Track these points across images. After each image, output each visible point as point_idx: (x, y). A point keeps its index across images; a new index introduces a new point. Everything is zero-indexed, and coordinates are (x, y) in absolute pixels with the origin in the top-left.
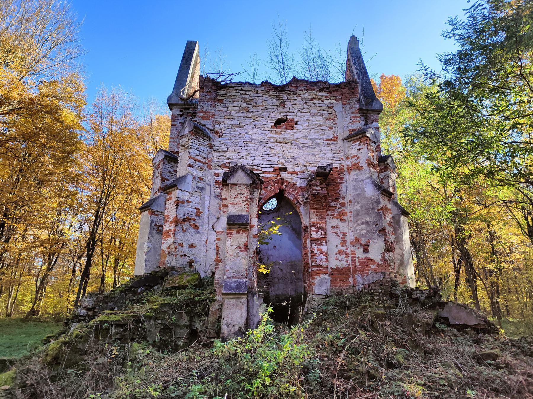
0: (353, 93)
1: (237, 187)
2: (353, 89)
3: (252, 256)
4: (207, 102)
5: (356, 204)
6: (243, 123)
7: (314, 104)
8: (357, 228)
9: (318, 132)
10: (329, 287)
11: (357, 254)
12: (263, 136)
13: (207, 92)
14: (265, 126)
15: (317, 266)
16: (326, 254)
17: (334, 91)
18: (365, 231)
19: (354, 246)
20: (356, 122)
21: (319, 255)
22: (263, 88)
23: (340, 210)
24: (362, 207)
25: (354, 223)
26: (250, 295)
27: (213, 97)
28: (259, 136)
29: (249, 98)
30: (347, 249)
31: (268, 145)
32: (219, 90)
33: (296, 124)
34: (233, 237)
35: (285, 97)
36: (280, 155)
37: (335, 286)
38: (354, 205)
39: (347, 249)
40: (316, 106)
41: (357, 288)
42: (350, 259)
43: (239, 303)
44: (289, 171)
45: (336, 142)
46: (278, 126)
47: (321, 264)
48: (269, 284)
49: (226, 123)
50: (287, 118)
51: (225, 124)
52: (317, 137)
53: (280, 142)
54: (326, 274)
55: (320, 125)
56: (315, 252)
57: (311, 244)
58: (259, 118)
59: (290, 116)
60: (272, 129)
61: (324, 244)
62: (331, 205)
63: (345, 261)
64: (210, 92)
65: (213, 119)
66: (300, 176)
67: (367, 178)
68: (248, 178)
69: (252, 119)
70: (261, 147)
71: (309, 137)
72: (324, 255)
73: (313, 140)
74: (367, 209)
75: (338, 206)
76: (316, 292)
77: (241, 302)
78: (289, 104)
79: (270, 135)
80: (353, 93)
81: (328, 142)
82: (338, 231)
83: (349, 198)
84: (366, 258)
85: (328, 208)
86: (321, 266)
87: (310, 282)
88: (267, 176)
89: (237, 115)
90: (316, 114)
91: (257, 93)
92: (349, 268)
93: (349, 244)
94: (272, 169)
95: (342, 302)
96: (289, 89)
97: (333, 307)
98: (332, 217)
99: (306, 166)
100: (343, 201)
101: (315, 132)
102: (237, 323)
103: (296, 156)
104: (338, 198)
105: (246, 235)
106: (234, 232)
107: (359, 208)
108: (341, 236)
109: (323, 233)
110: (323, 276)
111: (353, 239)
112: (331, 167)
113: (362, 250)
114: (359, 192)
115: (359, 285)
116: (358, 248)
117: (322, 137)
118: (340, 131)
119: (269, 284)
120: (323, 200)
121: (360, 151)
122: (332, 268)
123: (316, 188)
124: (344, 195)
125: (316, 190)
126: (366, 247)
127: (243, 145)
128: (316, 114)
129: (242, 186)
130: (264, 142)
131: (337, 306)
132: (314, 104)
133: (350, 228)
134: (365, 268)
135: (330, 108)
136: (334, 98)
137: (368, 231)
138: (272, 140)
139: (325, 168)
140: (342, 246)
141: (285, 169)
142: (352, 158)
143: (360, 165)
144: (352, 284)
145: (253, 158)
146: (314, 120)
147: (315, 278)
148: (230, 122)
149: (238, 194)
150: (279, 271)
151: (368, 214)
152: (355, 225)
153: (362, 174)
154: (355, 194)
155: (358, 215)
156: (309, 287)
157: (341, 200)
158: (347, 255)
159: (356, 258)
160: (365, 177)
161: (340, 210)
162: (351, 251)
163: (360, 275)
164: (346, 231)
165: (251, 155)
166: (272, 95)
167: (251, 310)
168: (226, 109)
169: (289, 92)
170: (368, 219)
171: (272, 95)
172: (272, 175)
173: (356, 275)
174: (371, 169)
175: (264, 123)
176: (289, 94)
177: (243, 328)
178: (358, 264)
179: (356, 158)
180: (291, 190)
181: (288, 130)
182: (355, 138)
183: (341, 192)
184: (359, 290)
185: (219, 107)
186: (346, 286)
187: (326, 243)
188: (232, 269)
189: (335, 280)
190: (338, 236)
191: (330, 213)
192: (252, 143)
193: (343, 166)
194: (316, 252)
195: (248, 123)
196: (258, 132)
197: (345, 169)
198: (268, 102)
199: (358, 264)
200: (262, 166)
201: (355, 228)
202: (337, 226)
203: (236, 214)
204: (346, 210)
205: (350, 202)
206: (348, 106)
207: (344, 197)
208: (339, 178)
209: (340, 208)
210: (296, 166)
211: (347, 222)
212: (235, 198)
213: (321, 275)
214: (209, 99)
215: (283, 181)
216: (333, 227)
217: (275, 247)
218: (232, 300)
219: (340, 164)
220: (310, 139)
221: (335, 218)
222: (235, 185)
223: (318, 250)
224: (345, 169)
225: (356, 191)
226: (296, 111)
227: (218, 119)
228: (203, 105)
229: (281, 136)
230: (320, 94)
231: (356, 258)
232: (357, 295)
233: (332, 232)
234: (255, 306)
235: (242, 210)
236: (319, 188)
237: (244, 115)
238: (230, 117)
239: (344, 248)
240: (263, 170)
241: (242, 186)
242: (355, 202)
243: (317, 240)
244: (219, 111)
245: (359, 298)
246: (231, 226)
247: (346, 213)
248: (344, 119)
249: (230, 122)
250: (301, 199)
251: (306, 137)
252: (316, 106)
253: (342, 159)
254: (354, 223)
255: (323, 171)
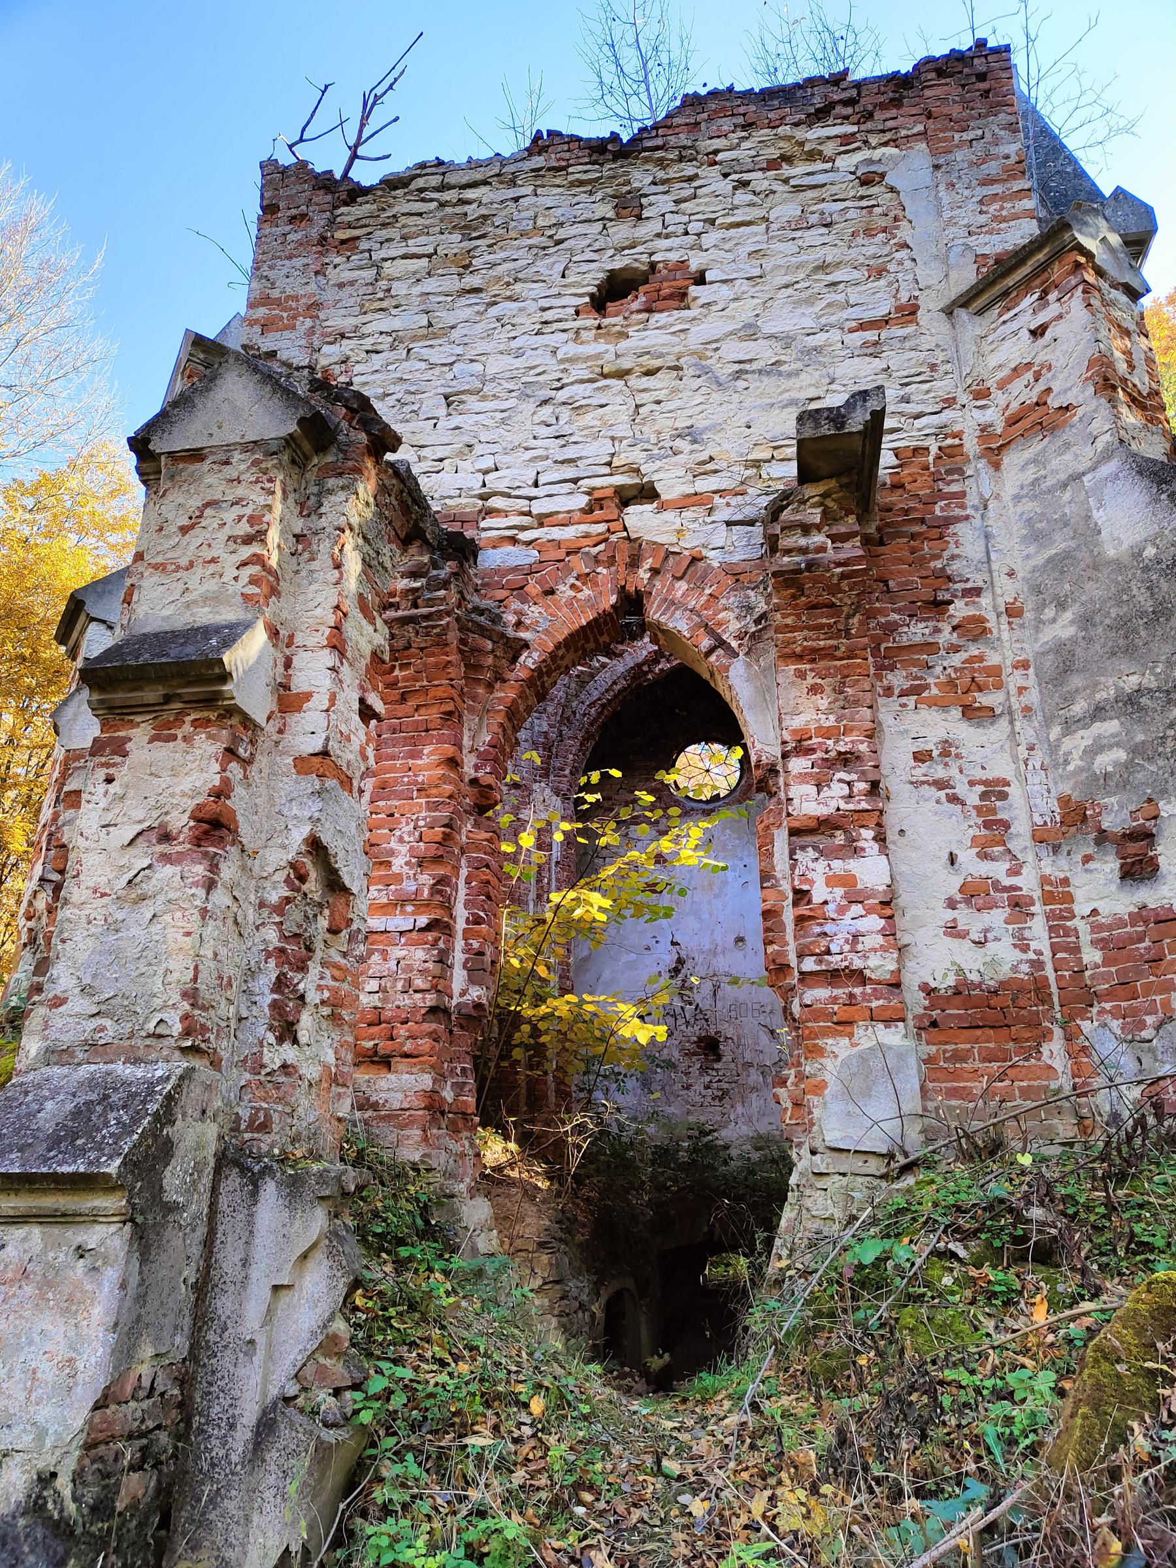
0: (986, 94)
1: (206, 466)
2: (982, 77)
3: (274, 897)
4: (290, 258)
5: (1049, 613)
6: (445, 317)
7: (786, 181)
8: (1067, 744)
9: (810, 301)
10: (912, 1103)
11: (1078, 894)
12: (542, 359)
13: (292, 220)
14: (548, 316)
15: (833, 976)
16: (887, 905)
17: (883, 106)
18: (1121, 755)
19: (1056, 849)
20: (1016, 217)
21: (842, 910)
22: (538, 161)
23: (957, 659)
24: (1086, 621)
25: (1048, 723)
26: (233, 1181)
27: (314, 232)
28: (518, 363)
29: (472, 211)
30: (1014, 872)
31: (562, 396)
32: (346, 204)
33: (700, 279)
34: (123, 774)
35: (640, 177)
36: (622, 430)
37: (953, 1093)
38: (1039, 624)
39: (1014, 872)
40: (799, 189)
41: (1103, 1102)
42: (1038, 930)
43: (63, 1256)
44: (664, 497)
45: (910, 329)
46: (611, 307)
47: (858, 963)
48: (725, 1093)
49: (366, 330)
50: (653, 266)
51: (361, 337)
52: (809, 323)
53: (622, 374)
54: (888, 1022)
55: (823, 267)
56: (817, 898)
57: (792, 853)
58: (518, 287)
59: (668, 252)
60: (578, 324)
61: (871, 847)
62: (904, 641)
63: (1008, 941)
64: (303, 216)
65: (309, 323)
66: (723, 514)
67: (1106, 455)
68: (276, 404)
69: (486, 297)
70: (529, 407)
71: (767, 329)
72: (869, 911)
73: (787, 340)
74: (1123, 626)
75: (946, 636)
76: (833, 1137)
77: (81, 1252)
78: (659, 204)
79: (571, 349)
80: (986, 94)
81: (871, 336)
82: (954, 771)
83: (1007, 590)
84: (1141, 914)
85: (887, 661)
86: (859, 976)
87: (801, 1077)
88: (556, 533)
89: (417, 290)
90: (800, 225)
91: (513, 183)
92: (1040, 989)
93: (1027, 841)
94: (582, 501)
95: (996, 1206)
96: (659, 142)
97: (930, 1242)
98: (911, 701)
99: (757, 464)
100: (971, 611)
101: (798, 303)
102: (27, 1440)
103: (700, 423)
104: (943, 596)
105: (217, 748)
106: (139, 735)
107: (1071, 631)
108: (972, 797)
109: (861, 786)
110: (868, 1036)
111: (1047, 808)
112: (873, 404)
113: (1110, 865)
114: (1060, 544)
115: (1112, 1085)
116: (1087, 859)
117: (833, 319)
118: (929, 274)
119: (725, 1093)
120: (846, 599)
121: (1049, 334)
122: (929, 991)
123: (803, 542)
124: (977, 580)
125: (803, 551)
126: (1133, 847)
127: (442, 411)
128: (800, 225)
129: (237, 456)
130: (542, 386)
131: (965, 1236)
132: (786, 181)
133: (1022, 752)
134: (1140, 973)
135: (866, 181)
136: (888, 136)
137: (1136, 750)
138: (580, 371)
139: (837, 416)
140: (984, 856)
141: (647, 493)
142: (1002, 385)
143: (1054, 402)
144: (1064, 1082)
145: (488, 462)
146: (791, 247)
147: (819, 1052)
148: (386, 323)
149: (208, 505)
150: (764, 1038)
151: (1129, 651)
152: (1055, 732)
153: (1067, 445)
154: (1040, 560)
155: (1066, 669)
156: (797, 1105)
157: (959, 610)
158: (1019, 906)
159: (1076, 923)
160: (1088, 453)
161: (957, 659)
162: (1045, 880)
163: (1116, 1025)
164: (1001, 768)
165: (479, 449)
166: (581, 183)
167: (224, 1304)
168: (370, 274)
169: (660, 154)
170: (1131, 682)
171: (581, 183)
172: (583, 528)
173: (1086, 1026)
174: (1124, 410)
175: (545, 303)
176: (661, 163)
177: (64, 1484)
178: (1091, 955)
179: (1029, 376)
180: (682, 586)
181: (657, 316)
182: (1010, 281)
183: (955, 567)
184: (1115, 1117)
185: (342, 269)
186: (1026, 1093)
187: (880, 839)
188: (86, 990)
189: (958, 1057)
190: (954, 799)
191: (898, 679)
192: (484, 398)
193: (958, 435)
194: (819, 893)
195: (468, 313)
196: (514, 344)
197: (971, 445)
198: (558, 212)
199: (1091, 955)
200: (534, 492)
201: (1054, 748)
202: (947, 749)
203: (182, 621)
204: (993, 659)
205: (1013, 612)
206: (960, 155)
207: (977, 592)
208: (940, 495)
209: (955, 649)
210: (705, 467)
211: (1003, 723)
212: (184, 530)
213: (859, 1031)
214: (300, 243)
215: (635, 551)
216: (921, 757)
217: (740, 940)
218: (19, 1232)
219: (942, 431)
220: (771, 336)
221: (933, 703)
222: (196, 455)
223: (832, 881)
224: (971, 445)
225: (1042, 547)
226: (695, 227)
227: (337, 320)
228: (271, 274)
229: (624, 344)
230: (818, 132)
231: (1076, 923)
232: (1103, 1157)
233: (916, 784)
234: (255, 1273)
235: (214, 599)
236: (818, 539)
237: (453, 284)
238: (384, 304)
239: (998, 870)
240: (538, 508)
241: (237, 456)
242: (1040, 609)
243: (824, 825)
244: (341, 285)
245: (1121, 1178)
246: (119, 696)
247: (996, 671)
248: (947, 215)
249: (386, 323)
250: (735, 626)
251: (750, 332)
252: (799, 189)
253: (950, 402)
254: (1048, 723)
255: (827, 430)
